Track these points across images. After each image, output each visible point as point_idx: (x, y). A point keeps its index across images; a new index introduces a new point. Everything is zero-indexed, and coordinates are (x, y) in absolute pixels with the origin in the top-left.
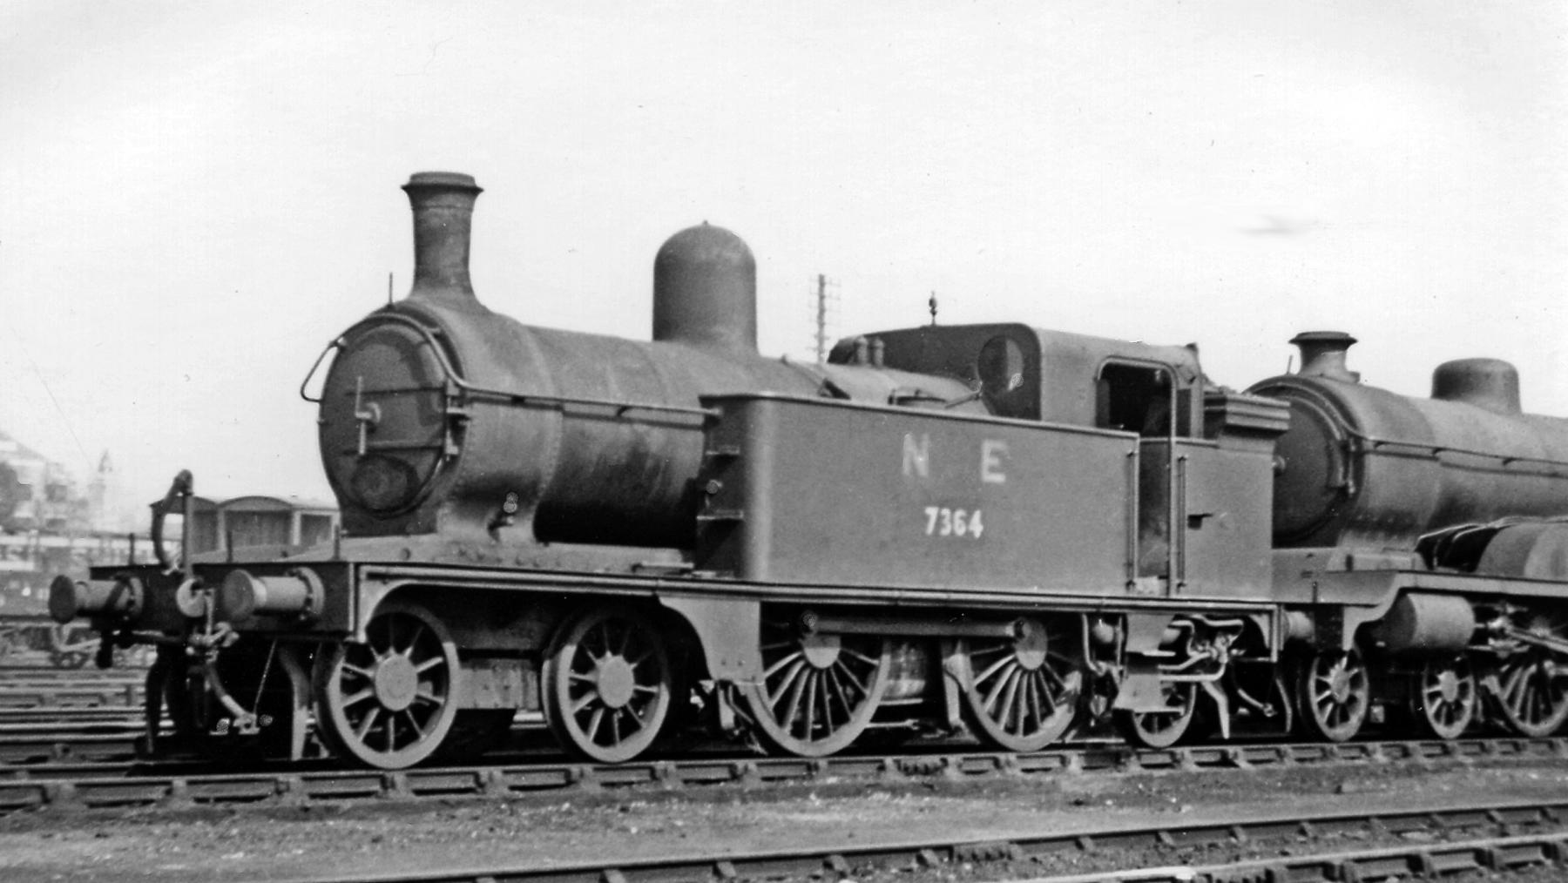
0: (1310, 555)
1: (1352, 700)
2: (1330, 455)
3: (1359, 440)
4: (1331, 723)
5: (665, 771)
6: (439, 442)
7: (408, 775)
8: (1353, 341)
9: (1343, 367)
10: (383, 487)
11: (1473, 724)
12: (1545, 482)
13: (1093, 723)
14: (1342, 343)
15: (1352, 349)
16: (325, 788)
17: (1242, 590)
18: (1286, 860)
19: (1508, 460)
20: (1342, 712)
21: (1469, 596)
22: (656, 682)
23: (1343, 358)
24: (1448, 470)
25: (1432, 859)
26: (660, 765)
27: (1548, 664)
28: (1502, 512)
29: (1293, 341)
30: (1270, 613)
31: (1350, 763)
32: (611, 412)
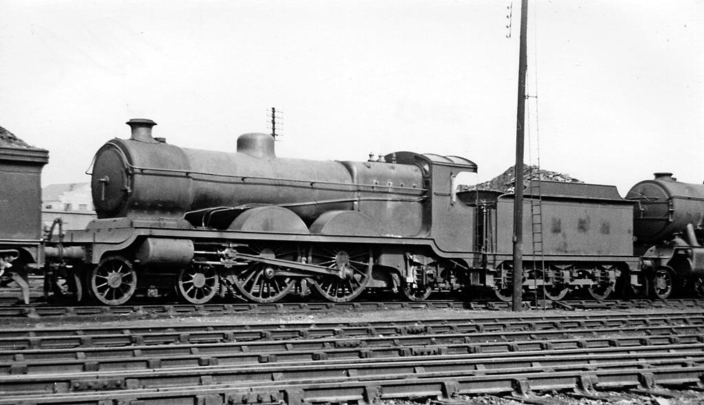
0: (115, 221)
1: (667, 288)
2: (122, 174)
3: (132, 169)
4: (660, 293)
5: (304, 306)
6: (666, 218)
7: (36, 309)
8: (155, 124)
9: (150, 136)
10: (113, 202)
11: (133, 297)
12: (274, 188)
13: (50, 294)
14: (149, 125)
15: (154, 127)
16: (79, 311)
17: (15, 236)
18: (650, 337)
19: (243, 179)
20: (663, 292)
21: (194, 239)
22: (213, 275)
23: (150, 132)
24: (195, 181)
25: (651, 340)
26: (355, 304)
27: (268, 270)
28: (241, 202)
29: (128, 123)
30: (36, 246)
31: (114, 315)
32: (308, 185)
